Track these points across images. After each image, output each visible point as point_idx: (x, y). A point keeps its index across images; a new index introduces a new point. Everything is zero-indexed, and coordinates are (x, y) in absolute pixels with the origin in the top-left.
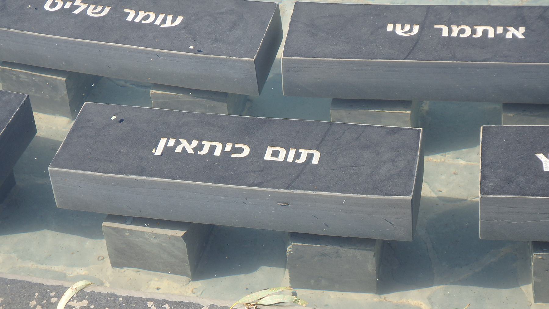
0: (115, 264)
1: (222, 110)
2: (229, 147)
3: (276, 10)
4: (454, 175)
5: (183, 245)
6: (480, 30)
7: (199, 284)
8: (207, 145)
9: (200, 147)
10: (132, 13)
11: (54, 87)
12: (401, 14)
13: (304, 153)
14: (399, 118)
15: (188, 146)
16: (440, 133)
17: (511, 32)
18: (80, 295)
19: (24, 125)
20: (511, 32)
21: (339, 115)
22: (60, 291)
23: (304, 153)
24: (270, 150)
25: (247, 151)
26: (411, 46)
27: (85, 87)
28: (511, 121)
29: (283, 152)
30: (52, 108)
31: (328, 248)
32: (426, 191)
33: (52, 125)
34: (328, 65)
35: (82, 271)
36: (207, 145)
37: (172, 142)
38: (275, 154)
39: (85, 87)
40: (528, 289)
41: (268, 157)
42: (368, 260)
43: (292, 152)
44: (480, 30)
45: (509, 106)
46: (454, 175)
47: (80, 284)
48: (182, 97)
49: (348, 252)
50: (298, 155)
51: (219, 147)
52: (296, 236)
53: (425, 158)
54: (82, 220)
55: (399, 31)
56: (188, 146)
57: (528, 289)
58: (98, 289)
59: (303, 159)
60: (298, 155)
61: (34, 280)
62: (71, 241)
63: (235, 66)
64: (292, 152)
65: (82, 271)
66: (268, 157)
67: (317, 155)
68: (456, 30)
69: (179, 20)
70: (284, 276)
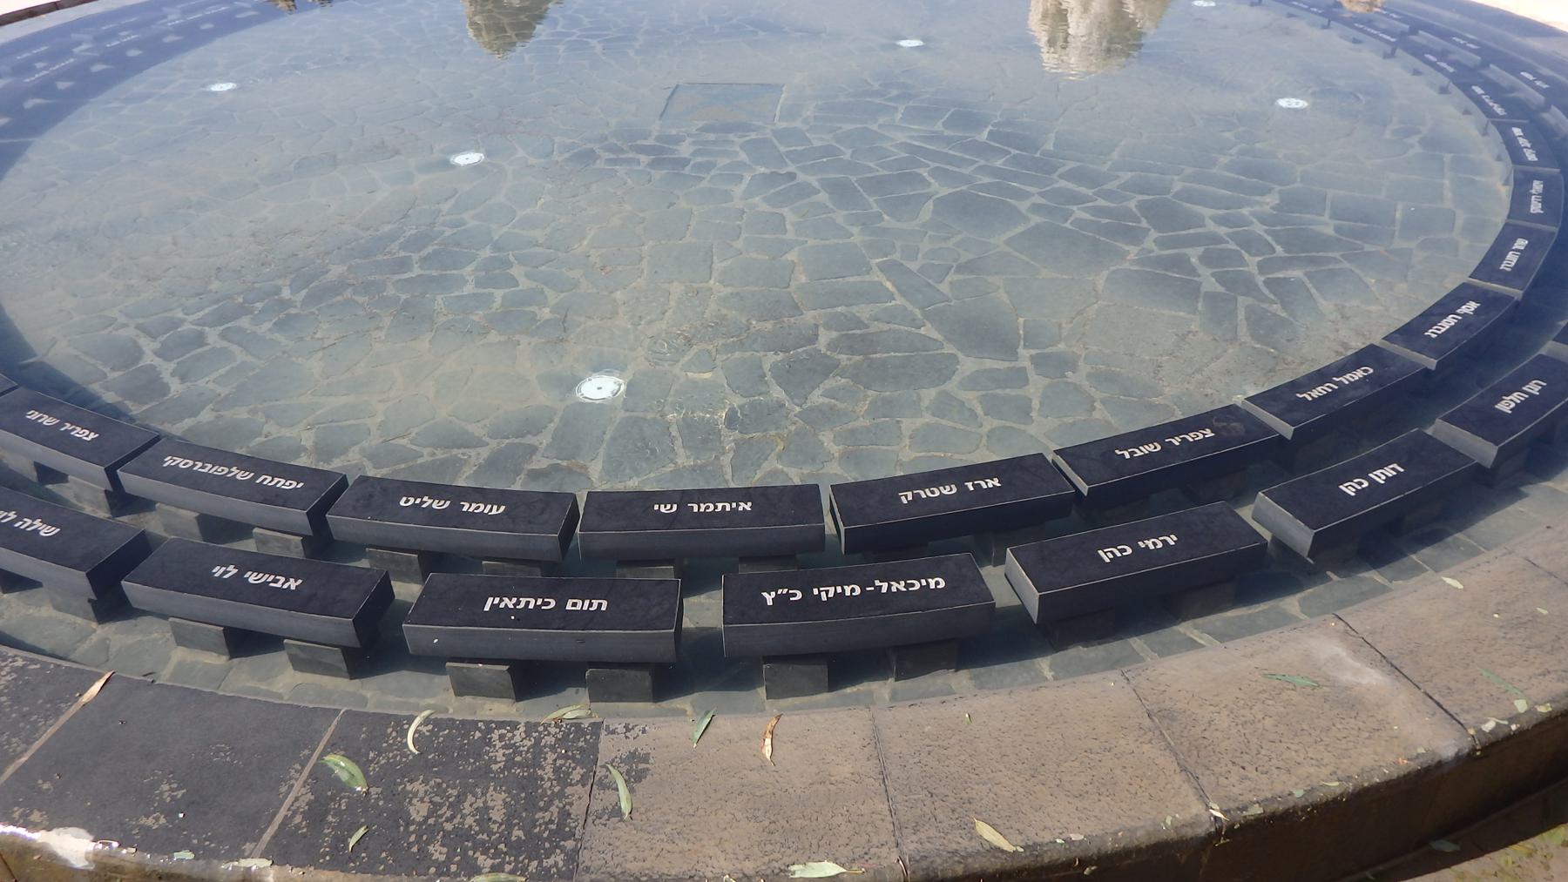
0: (458, 693)
1: (537, 574)
2: (540, 602)
3: (574, 497)
4: (704, 611)
5: (508, 677)
6: (720, 506)
7: (357, 681)
8: (523, 601)
9: (519, 602)
10: (467, 505)
11: (409, 561)
12: (663, 497)
13: (596, 603)
14: (667, 573)
15: (509, 603)
16: (694, 582)
17: (1380, 476)
18: (426, 721)
19: (384, 592)
20: (1380, 476)
21: (631, 575)
22: (410, 720)
23: (596, 603)
24: (570, 602)
25: (553, 603)
26: (670, 520)
27: (433, 561)
28: (745, 570)
29: (580, 602)
30: (406, 577)
31: (617, 671)
32: (687, 623)
33: (406, 591)
34: (611, 536)
35: (431, 701)
36: (523, 601)
37: (497, 600)
38: (574, 605)
39: (433, 561)
40: (762, 691)
41: (569, 607)
42: (645, 679)
43: (587, 602)
44: (720, 506)
45: (743, 559)
46: (704, 611)
47: (427, 713)
48: (506, 565)
49: (631, 673)
50: (591, 605)
51: (532, 601)
52: (592, 664)
53: (685, 601)
54: (430, 662)
55: (663, 510)
56: (509, 603)
57: (762, 691)
58: (440, 716)
59: (594, 607)
60: (591, 605)
61: (391, 712)
62: (421, 678)
63: (545, 539)
64: (587, 602)
65: (431, 701)
66: (569, 607)
67: (605, 603)
68: (703, 507)
69: (502, 508)
70: (584, 694)
